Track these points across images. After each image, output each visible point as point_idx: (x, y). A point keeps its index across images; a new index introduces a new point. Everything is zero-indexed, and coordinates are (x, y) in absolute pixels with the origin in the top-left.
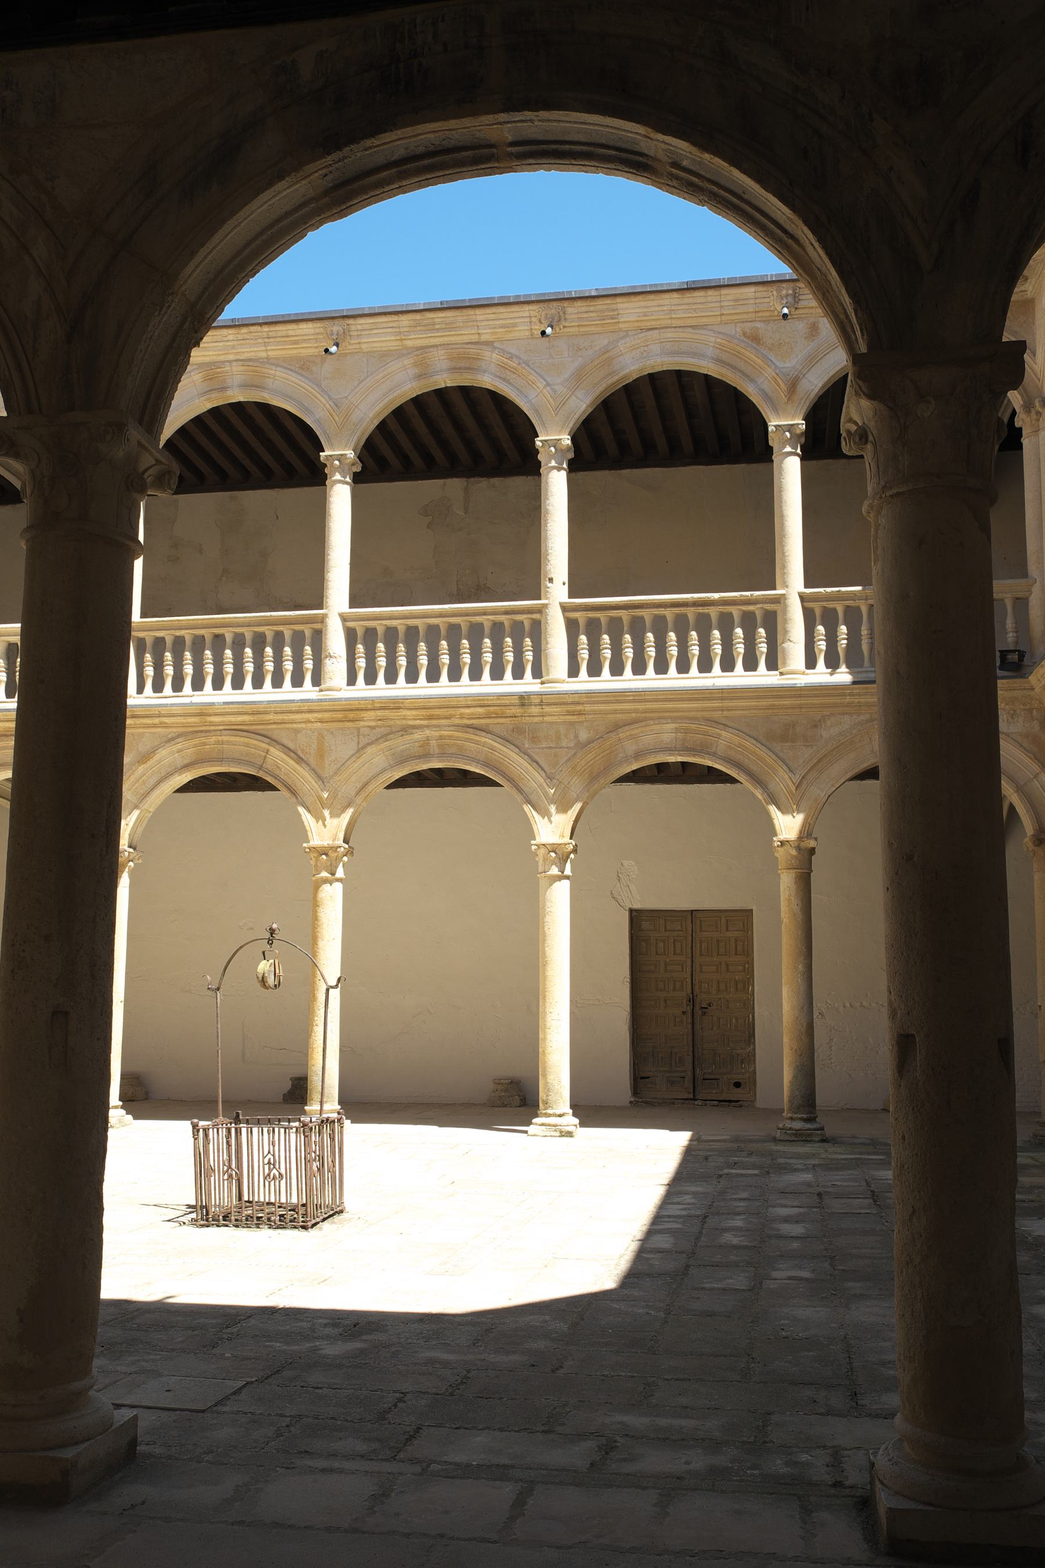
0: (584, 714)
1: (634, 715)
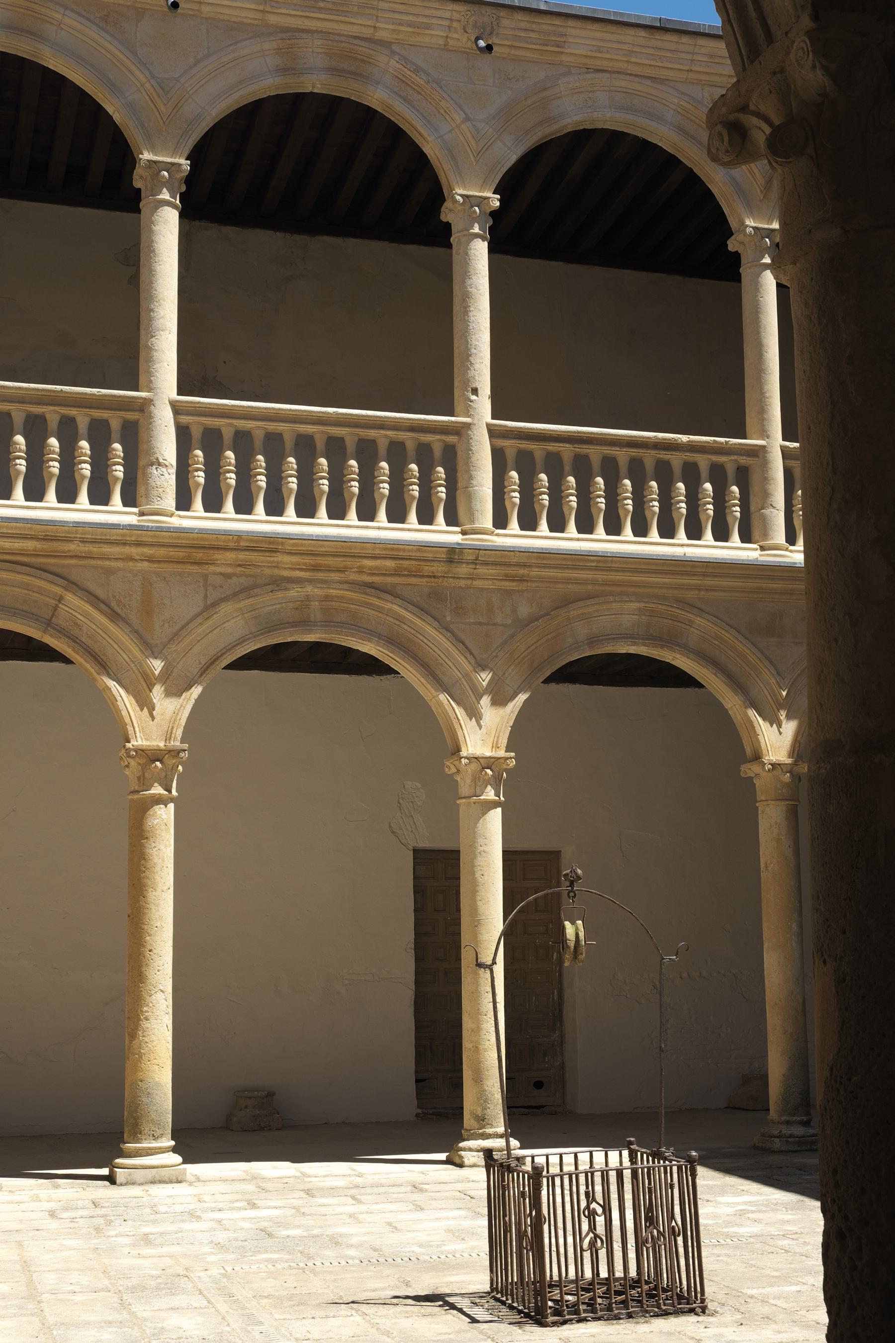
0: (527, 581)
1: (590, 587)
